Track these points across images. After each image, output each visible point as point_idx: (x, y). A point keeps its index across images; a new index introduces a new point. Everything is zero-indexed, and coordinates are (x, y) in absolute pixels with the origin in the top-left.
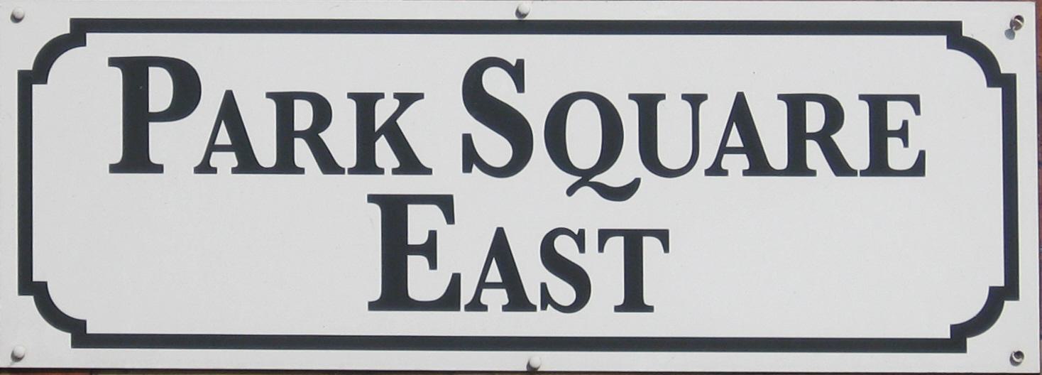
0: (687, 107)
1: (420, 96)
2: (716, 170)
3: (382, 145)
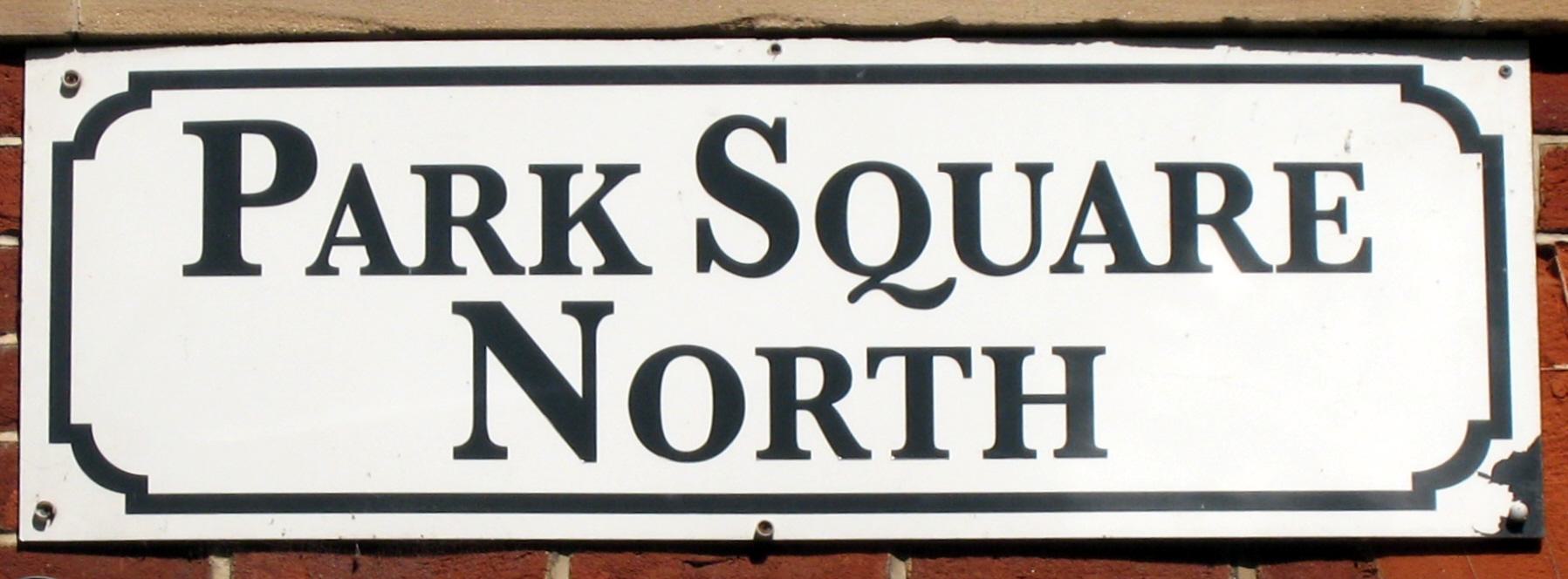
0: (1024, 181)
1: (634, 169)
2: (1066, 265)
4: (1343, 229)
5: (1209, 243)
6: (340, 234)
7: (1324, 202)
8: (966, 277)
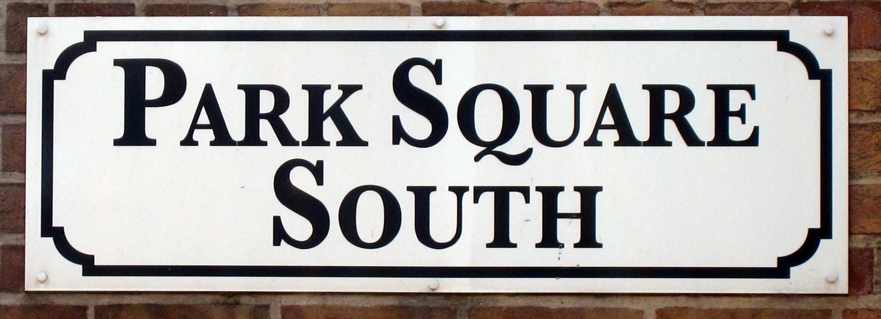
0: (571, 95)
1: (359, 87)
2: (593, 142)
4: (743, 122)
5: (670, 129)
6: (603, 123)
7: (734, 106)
8: (539, 148)
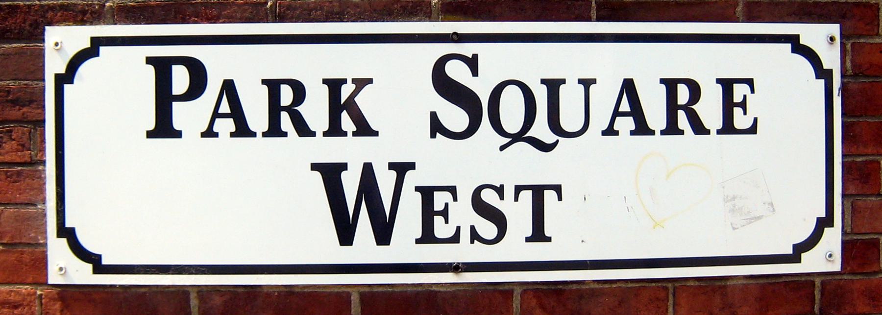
0: (581, 88)
1: (370, 81)
2: (610, 131)
3: (345, 117)
